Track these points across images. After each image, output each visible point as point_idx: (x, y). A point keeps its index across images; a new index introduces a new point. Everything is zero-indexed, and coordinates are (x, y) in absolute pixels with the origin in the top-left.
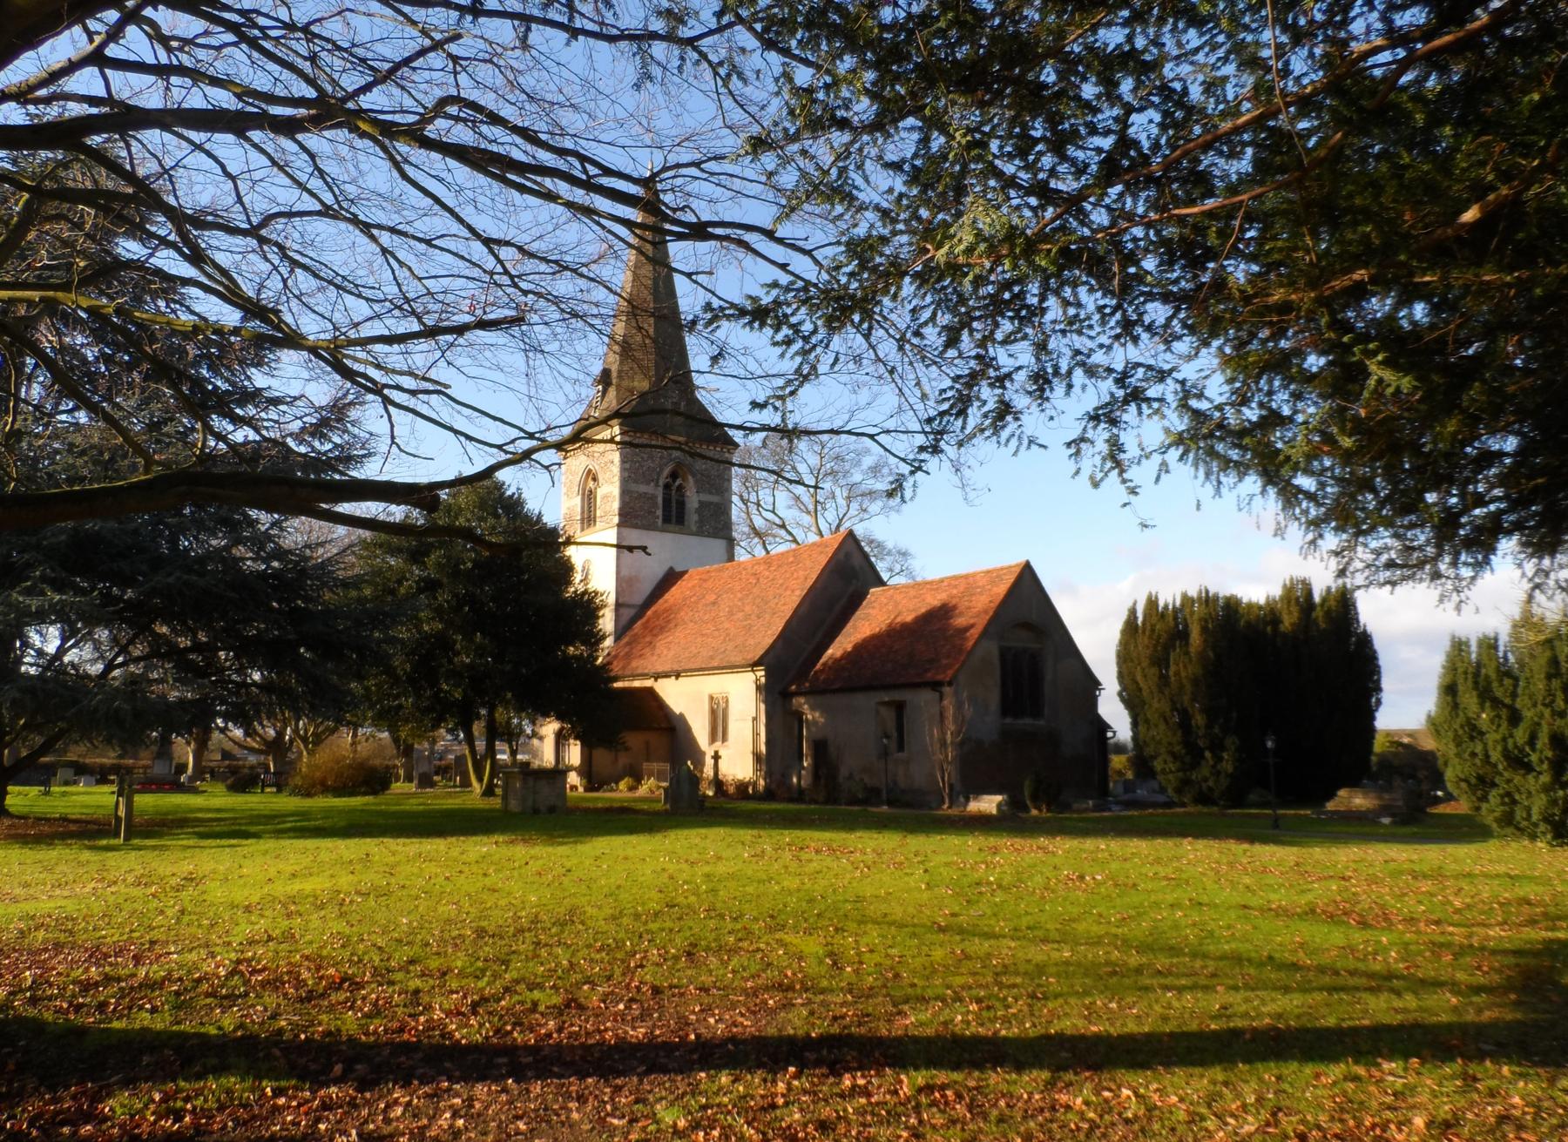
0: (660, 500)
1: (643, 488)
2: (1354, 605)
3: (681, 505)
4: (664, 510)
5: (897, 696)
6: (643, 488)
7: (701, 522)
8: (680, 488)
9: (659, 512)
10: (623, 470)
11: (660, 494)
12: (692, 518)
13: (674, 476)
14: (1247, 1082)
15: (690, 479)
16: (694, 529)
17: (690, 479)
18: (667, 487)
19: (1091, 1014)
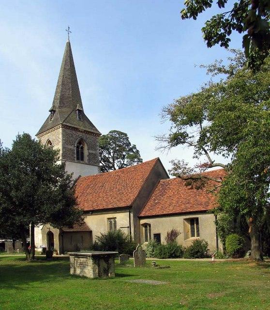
0: (75, 151)
1: (70, 147)
2: (37, 281)
3: (82, 153)
4: (77, 156)
5: (168, 172)
6: (70, 147)
7: (89, 160)
8: (82, 148)
9: (75, 156)
10: (63, 140)
11: (75, 149)
12: (86, 158)
13: (80, 143)
14: (228, 78)
15: (86, 145)
16: (87, 162)
17: (86, 145)
18: (78, 147)
19: (57, 244)
